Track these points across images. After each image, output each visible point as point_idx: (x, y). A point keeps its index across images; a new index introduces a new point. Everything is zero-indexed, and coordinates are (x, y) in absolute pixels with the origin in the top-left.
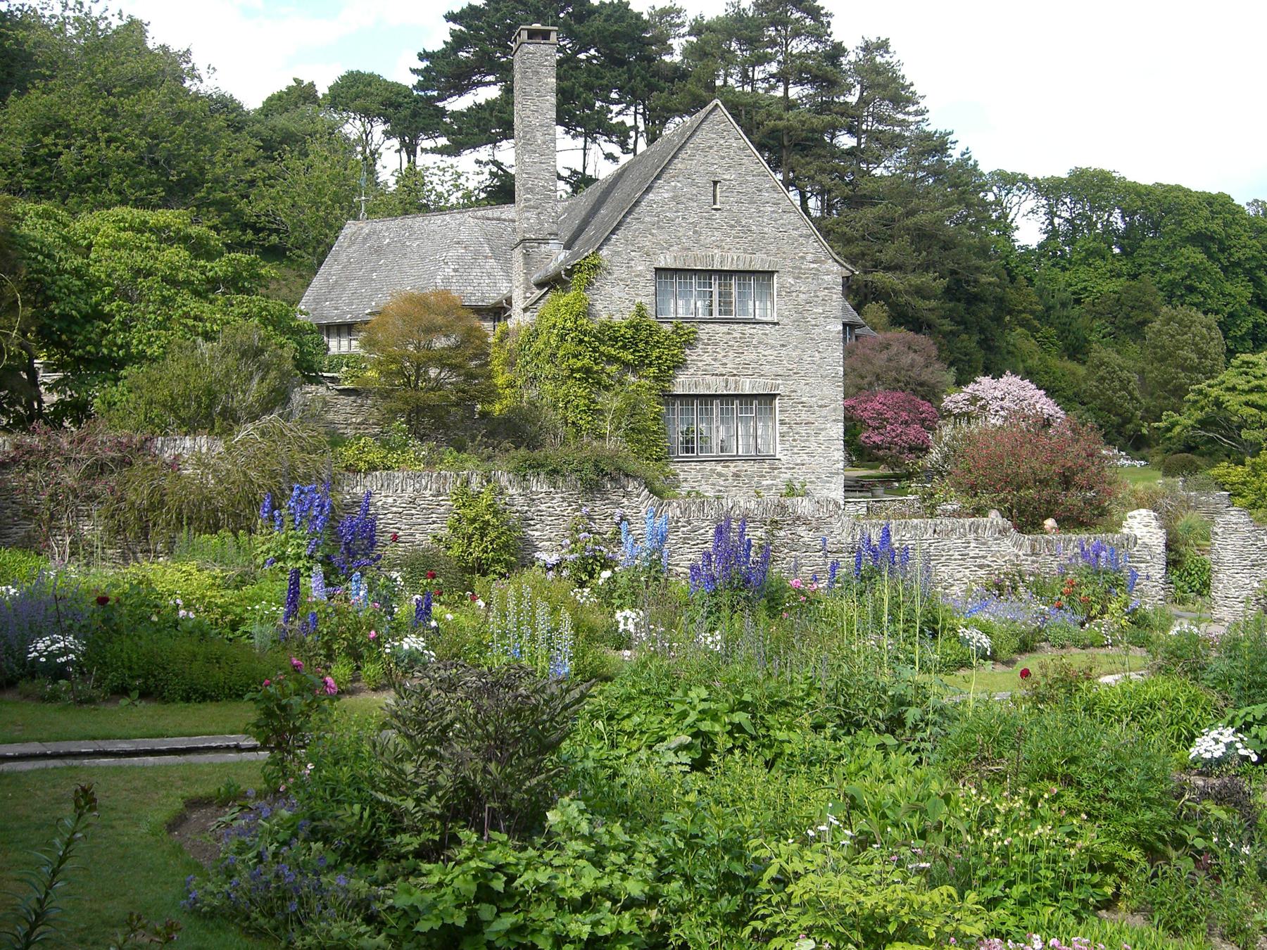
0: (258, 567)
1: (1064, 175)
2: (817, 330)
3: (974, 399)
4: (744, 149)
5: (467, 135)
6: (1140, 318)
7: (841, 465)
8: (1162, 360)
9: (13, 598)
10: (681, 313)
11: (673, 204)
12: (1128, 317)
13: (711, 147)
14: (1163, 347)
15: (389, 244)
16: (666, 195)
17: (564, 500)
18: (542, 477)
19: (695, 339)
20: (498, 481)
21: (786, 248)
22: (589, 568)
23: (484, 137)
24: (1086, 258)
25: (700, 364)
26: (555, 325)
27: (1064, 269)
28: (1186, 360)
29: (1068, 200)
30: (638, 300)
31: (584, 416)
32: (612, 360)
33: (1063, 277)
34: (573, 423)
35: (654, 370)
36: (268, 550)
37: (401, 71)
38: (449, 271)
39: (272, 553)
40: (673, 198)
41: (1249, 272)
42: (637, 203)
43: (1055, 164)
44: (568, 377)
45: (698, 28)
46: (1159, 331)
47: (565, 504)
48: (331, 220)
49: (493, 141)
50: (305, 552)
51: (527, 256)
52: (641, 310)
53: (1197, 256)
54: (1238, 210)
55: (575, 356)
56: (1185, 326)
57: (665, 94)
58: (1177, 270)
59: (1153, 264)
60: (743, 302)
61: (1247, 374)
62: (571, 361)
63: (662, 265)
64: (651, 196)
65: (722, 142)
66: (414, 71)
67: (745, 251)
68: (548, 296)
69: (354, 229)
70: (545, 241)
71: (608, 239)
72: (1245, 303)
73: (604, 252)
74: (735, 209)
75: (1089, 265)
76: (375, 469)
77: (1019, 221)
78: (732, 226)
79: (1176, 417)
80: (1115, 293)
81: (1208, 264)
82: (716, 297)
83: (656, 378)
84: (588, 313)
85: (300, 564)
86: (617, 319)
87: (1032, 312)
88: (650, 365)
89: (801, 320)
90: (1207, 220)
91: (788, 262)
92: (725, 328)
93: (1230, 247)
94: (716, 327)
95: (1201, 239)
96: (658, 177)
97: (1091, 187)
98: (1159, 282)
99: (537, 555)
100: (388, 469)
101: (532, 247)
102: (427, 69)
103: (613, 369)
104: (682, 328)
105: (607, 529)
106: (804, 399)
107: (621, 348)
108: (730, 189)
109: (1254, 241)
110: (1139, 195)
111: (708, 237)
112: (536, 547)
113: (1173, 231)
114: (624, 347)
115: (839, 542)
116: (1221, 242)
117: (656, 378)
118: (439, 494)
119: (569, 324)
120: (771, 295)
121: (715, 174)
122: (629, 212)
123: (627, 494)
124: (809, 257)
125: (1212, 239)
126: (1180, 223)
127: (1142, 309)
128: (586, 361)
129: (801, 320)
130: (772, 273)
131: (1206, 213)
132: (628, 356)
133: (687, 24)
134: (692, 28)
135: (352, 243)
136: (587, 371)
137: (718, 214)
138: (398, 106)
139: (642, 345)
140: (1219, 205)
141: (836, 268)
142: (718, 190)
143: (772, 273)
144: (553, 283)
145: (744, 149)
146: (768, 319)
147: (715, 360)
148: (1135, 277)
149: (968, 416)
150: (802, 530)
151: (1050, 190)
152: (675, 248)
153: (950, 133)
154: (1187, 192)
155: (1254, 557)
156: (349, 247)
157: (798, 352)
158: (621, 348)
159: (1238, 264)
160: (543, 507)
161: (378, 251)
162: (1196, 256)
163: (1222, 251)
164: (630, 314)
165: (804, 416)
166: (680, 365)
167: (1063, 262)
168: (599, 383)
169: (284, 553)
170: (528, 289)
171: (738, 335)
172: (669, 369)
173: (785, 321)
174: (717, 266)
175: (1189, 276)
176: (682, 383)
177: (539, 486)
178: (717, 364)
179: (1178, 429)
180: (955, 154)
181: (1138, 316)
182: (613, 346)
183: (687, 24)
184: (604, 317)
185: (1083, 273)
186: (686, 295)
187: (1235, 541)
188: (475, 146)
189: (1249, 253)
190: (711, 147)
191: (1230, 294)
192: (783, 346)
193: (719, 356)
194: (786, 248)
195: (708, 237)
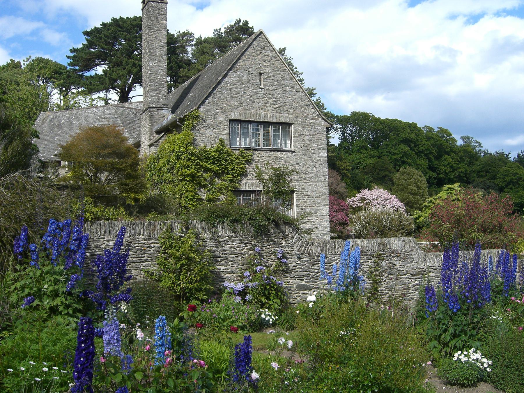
0: (13, 306)
1: (348, 114)
2: (314, 156)
3: (363, 200)
4: (275, 57)
5: (94, 85)
6: (384, 174)
7: (328, 229)
8: (402, 190)
10: (243, 145)
11: (238, 84)
12: (378, 174)
13: (258, 55)
14: (402, 185)
15: (63, 123)
16: (235, 79)
17: (241, 242)
18: (226, 225)
19: (251, 159)
20: (194, 227)
21: (298, 111)
22: (267, 292)
23: (102, 86)
24: (359, 150)
26: (174, 150)
27: (350, 154)
28: (412, 190)
29: (350, 126)
30: (220, 137)
31: (191, 202)
32: (206, 170)
34: (185, 207)
35: (230, 176)
36: (23, 288)
37: (61, 58)
39: (27, 291)
40: (239, 81)
41: (426, 155)
42: (219, 83)
44: (181, 180)
45: (200, 42)
46: (399, 178)
47: (243, 245)
48: (31, 115)
49: (107, 89)
50: (62, 288)
51: (151, 116)
52: (222, 142)
53: (406, 148)
54: (419, 129)
55: (186, 168)
56: (410, 175)
57: (186, 70)
58: (398, 154)
59: (387, 152)
60: (275, 141)
62: (184, 171)
63: (233, 117)
64: (227, 79)
65: (264, 52)
66: (68, 57)
67: (277, 112)
68: (164, 138)
69: (45, 116)
70: (161, 108)
71: (203, 102)
72: (425, 168)
73: (201, 109)
74: (271, 88)
75: (361, 153)
76: (99, 219)
78: (270, 98)
79: (420, 213)
80: (373, 164)
82: (261, 136)
83: (231, 181)
84: (193, 143)
85: (57, 301)
86: (209, 147)
88: (228, 173)
89: (306, 151)
91: (299, 119)
92: (266, 154)
93: (418, 145)
94: (263, 153)
95: (407, 141)
96: (231, 69)
98: (390, 160)
99: (226, 284)
100: (108, 219)
101: (154, 111)
102: (74, 56)
103: (207, 175)
104: (244, 153)
105: (272, 263)
106: (309, 193)
107: (211, 163)
108: (268, 78)
109: (428, 142)
111: (258, 104)
112: (222, 278)
113: (395, 138)
114: (213, 163)
115: (417, 268)
116: (415, 143)
117: (231, 181)
118: (149, 238)
119: (182, 149)
120: (290, 136)
121: (260, 69)
122: (215, 88)
123: (285, 237)
124: (310, 116)
125: (411, 141)
126: (398, 135)
128: (192, 170)
129: (306, 151)
130: (289, 125)
131: (408, 130)
132: (215, 168)
133: (195, 40)
134: (197, 42)
135: (44, 123)
136: (193, 176)
137: (262, 91)
138: (61, 73)
139: (223, 162)
140: (412, 127)
141: (323, 122)
142: (262, 78)
143: (289, 125)
144: (166, 130)
145: (275, 57)
146: (289, 148)
148: (379, 157)
149: (359, 209)
150: (395, 260)
152: (240, 108)
153: (315, 89)
154: (400, 122)
156: (42, 124)
157: (305, 168)
158: (211, 163)
160: (227, 247)
161: (58, 126)
162: (405, 148)
163: (415, 146)
164: (216, 144)
165: (309, 202)
166: (244, 174)
167: (349, 151)
168: (199, 183)
169: (40, 290)
170: (151, 134)
171: (274, 158)
172: (238, 176)
174: (262, 119)
175: (403, 157)
177: (224, 232)
179: (422, 219)
181: (383, 173)
182: (207, 162)
183: (195, 40)
184: (202, 145)
185: (358, 155)
186: (245, 135)
188: (97, 91)
189: (427, 147)
190: (258, 55)
191: (419, 164)
192: (297, 164)
194: (298, 111)
195: (258, 104)
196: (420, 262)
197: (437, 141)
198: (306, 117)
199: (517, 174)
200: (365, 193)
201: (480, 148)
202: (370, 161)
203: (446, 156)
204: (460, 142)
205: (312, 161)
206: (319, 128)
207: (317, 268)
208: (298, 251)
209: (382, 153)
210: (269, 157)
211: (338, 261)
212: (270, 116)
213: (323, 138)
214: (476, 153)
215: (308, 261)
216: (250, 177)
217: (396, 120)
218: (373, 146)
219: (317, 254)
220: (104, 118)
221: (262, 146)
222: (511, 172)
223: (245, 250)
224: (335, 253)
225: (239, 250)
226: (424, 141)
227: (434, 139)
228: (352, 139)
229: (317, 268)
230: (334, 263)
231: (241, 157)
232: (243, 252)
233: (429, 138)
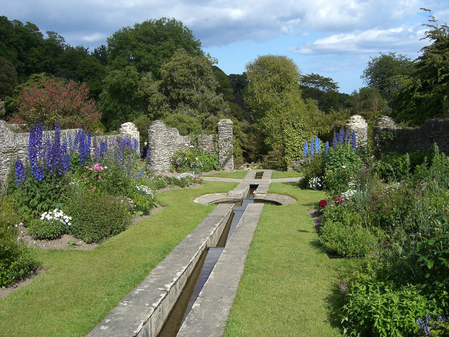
9: (63, 50)
28: (3, 78)
41: (15, 47)
61: (38, 81)
72: (15, 58)
79: (11, 99)
93: (9, 37)
109: (17, 35)
155: (168, 141)
159: (11, 43)
163: (6, 38)
187: (161, 134)
189: (16, 39)
191: (9, 55)
197: (26, 34)
199: (94, 66)
201: (63, 43)
204: (46, 37)
226: (14, 34)
227: (23, 32)
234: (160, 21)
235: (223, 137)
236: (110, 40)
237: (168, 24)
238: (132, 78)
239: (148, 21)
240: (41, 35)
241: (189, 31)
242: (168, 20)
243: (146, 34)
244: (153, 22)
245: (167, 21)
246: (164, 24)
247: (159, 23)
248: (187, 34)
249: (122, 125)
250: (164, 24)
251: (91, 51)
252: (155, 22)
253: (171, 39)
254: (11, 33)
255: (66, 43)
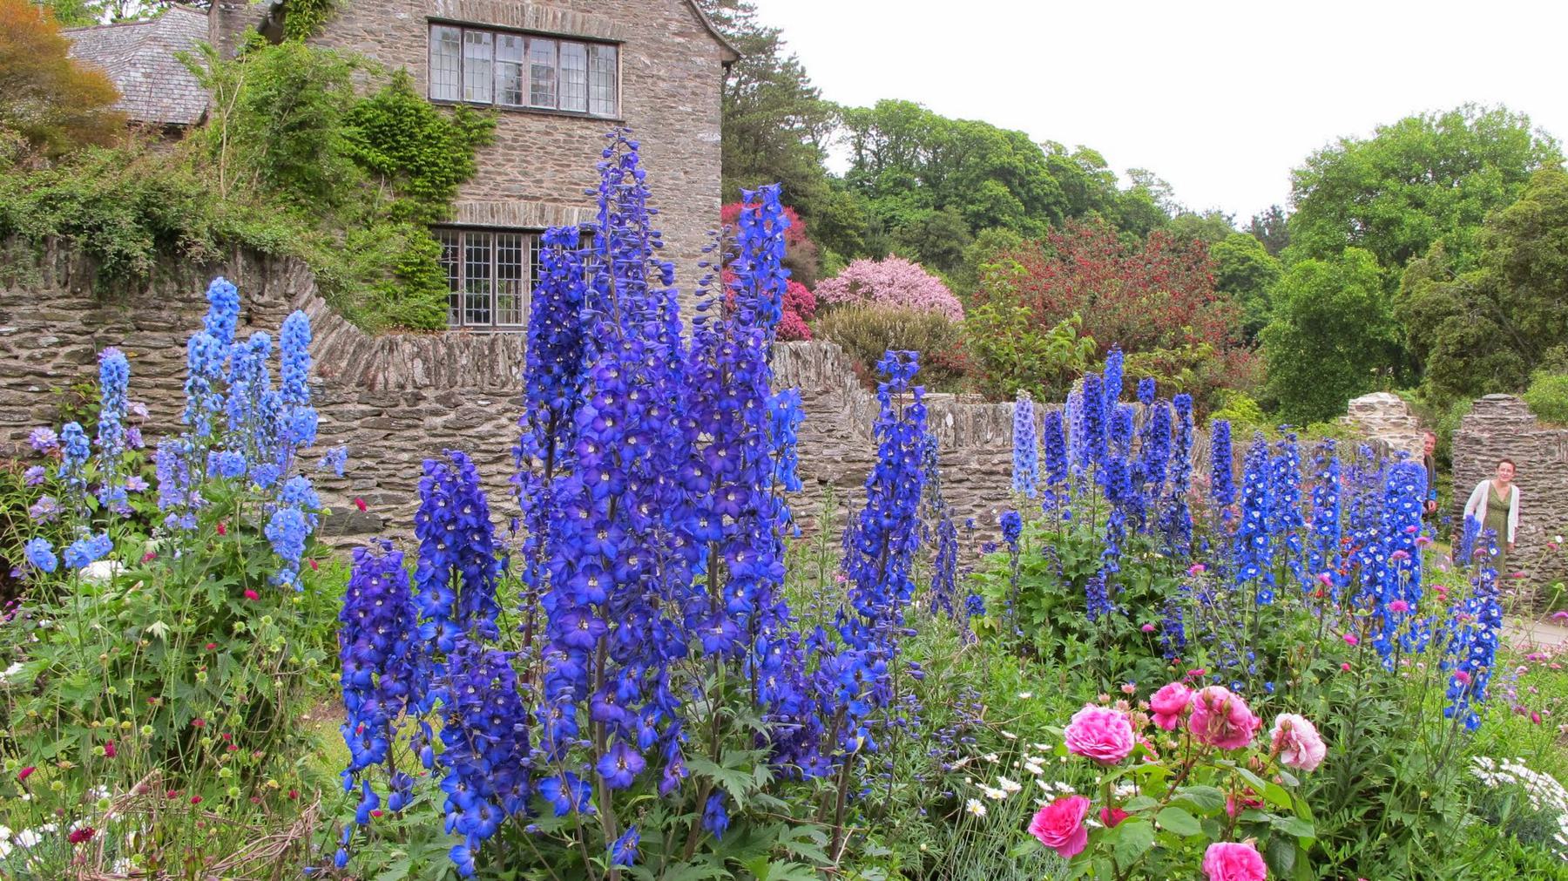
2: (683, 139)
12: (934, 245)
25: (499, 179)
30: (397, 67)
33: (873, 206)
38: (137, 75)
41: (1046, 207)
43: (863, 98)
77: (829, 150)
81: (1010, 198)
87: (856, 228)
90: (1009, 155)
94: (527, 121)
95: (1005, 174)
97: (897, 121)
110: (944, 125)
116: (1022, 178)
124: (674, 26)
126: (983, 157)
127: (948, 238)
131: (1009, 148)
140: (1016, 141)
146: (612, 116)
147: (525, 174)
151: (858, 121)
154: (991, 128)
162: (998, 189)
171: (561, 137)
173: (635, 120)
176: (467, 207)
178: (527, 182)
180: (782, 55)
181: (945, 245)
185: (891, 201)
193: (531, 169)
196: (856, 437)
198: (664, 27)
199: (1249, 259)
200: (863, 267)
202: (920, 215)
203: (1094, 212)
204: (1124, 184)
205: (676, 152)
206: (699, 60)
207: (408, 445)
208: (321, 374)
209: (945, 197)
210: (548, 133)
211: (504, 421)
212: (555, 17)
213: (710, 90)
214: (1161, 210)
215: (364, 414)
216: (486, 189)
217: (982, 123)
218: (926, 179)
219: (409, 389)
220: (154, 39)
221: (527, 102)
222: (1236, 253)
223: (59, 360)
224: (496, 389)
225: (31, 358)
228: (880, 162)
229: (408, 445)
230: (487, 427)
231: (459, 130)
232: (48, 368)
233: (1055, 169)
234: (1456, 114)
235: (318, 351)
236: (1298, 172)
237: (1480, 125)
238: (1363, 282)
239: (1417, 116)
240: (1111, 177)
241: (1552, 142)
242: (1483, 110)
243: (1413, 153)
244: (1432, 119)
245: (1478, 114)
246: (1468, 123)
247: (1452, 122)
248: (1541, 148)
249: (1352, 403)
250: (1468, 123)
251: (1242, 223)
252: (1438, 117)
253: (1487, 168)
254: (1037, 173)
255: (1175, 200)
